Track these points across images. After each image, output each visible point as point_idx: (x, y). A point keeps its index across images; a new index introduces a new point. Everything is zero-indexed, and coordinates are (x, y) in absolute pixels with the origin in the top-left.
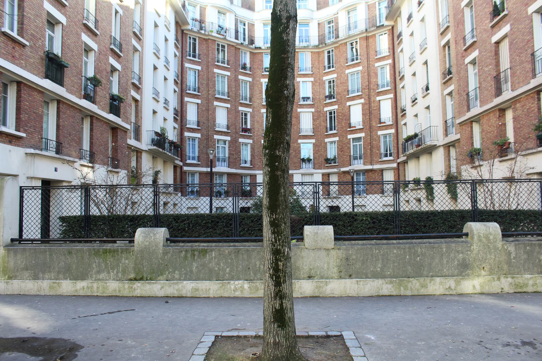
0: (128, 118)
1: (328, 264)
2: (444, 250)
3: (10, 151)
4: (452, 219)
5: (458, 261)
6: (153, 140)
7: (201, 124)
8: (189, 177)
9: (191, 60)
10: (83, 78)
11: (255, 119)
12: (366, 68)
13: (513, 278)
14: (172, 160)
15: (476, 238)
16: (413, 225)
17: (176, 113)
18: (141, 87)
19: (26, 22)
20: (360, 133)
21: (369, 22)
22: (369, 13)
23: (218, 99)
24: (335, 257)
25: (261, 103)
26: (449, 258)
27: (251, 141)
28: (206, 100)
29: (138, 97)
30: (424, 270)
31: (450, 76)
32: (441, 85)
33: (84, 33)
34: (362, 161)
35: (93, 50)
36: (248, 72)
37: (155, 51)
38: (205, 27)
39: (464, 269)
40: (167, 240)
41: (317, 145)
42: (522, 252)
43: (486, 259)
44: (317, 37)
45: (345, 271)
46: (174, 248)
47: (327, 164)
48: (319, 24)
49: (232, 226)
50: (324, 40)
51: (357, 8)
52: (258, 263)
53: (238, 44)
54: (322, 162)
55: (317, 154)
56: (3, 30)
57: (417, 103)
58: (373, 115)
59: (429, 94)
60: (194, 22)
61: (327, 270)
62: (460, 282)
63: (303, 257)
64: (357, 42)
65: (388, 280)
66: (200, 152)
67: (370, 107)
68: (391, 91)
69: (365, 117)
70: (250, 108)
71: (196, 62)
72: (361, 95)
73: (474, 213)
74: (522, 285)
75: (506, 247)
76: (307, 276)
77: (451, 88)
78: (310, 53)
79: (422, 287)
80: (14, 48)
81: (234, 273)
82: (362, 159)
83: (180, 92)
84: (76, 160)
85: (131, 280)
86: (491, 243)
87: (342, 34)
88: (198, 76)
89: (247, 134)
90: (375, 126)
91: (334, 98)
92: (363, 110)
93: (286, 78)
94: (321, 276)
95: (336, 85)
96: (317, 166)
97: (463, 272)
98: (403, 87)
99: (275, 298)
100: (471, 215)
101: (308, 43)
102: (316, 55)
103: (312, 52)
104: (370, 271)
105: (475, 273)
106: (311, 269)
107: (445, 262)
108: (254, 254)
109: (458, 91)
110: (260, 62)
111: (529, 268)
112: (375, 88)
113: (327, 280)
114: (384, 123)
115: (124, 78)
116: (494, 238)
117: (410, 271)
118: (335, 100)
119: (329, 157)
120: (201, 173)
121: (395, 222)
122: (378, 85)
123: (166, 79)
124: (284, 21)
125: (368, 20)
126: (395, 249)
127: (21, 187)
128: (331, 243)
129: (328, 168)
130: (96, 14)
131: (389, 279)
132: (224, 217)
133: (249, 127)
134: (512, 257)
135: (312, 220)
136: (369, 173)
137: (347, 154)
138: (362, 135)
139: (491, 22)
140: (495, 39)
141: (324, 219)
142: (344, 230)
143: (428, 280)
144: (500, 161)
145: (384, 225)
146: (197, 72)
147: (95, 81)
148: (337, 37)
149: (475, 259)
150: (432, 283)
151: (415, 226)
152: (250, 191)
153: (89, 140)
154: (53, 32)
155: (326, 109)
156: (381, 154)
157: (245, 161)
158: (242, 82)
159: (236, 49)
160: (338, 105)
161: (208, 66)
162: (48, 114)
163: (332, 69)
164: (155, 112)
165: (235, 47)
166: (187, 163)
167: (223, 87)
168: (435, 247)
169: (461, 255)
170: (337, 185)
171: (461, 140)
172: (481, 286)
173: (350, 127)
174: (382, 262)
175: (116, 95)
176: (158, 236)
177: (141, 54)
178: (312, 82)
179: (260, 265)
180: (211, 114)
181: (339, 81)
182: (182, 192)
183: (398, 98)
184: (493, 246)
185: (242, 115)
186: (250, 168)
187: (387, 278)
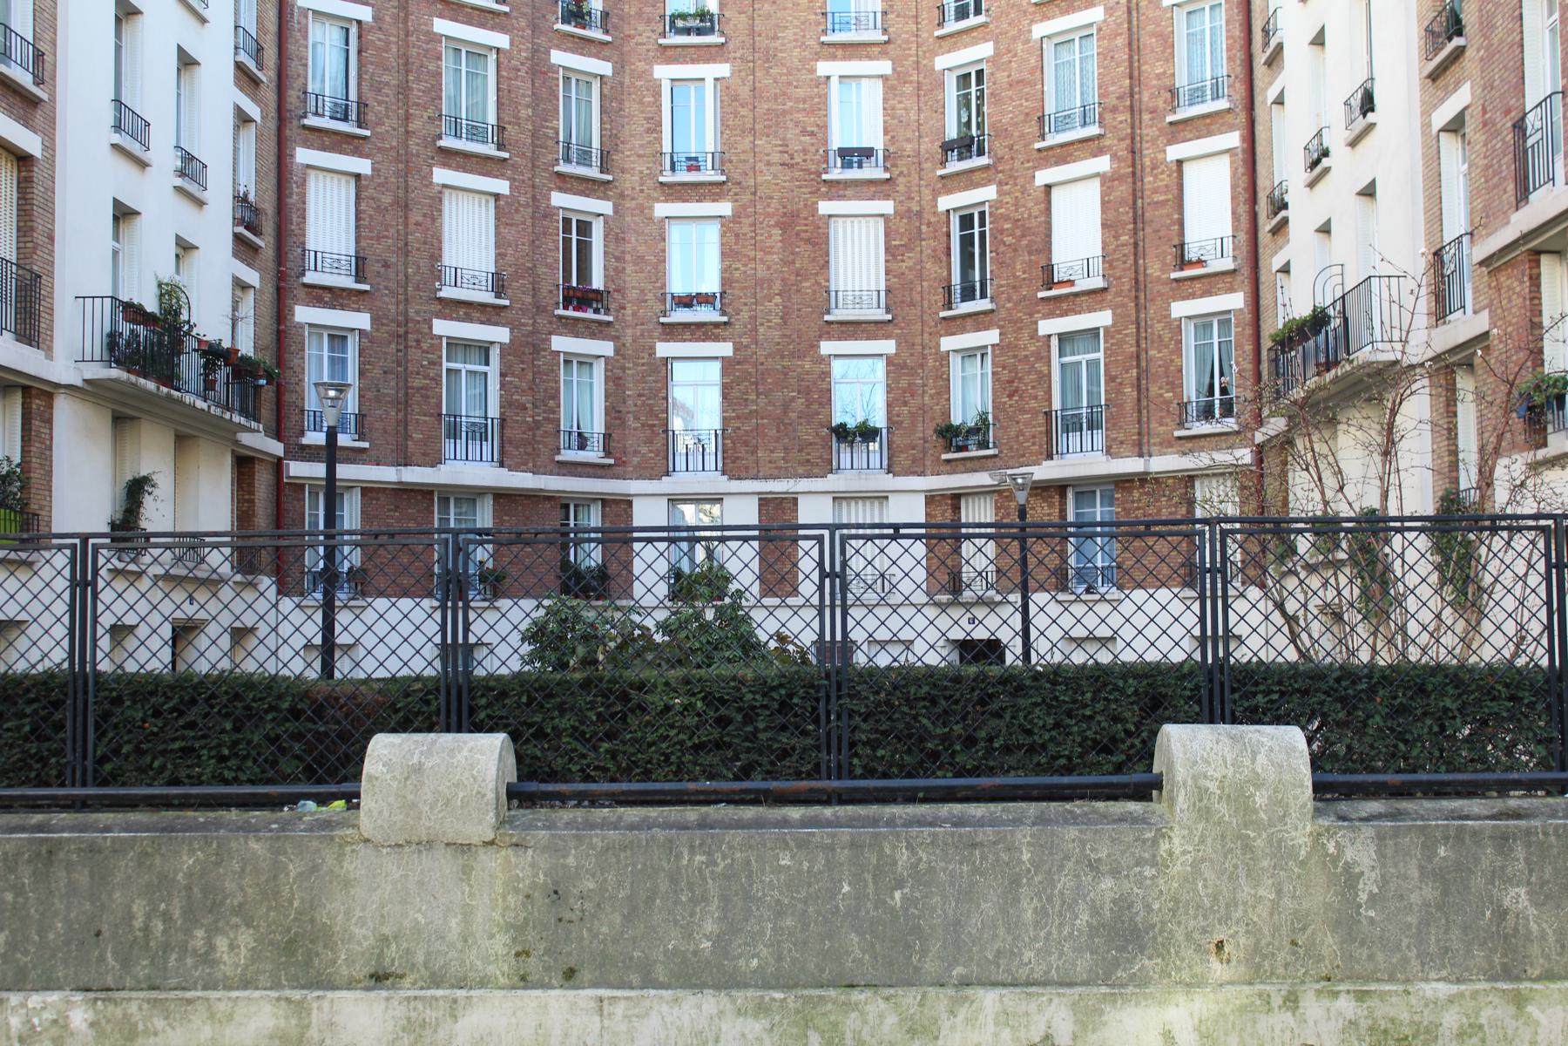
1: (467, 914)
2: (1026, 856)
4: (1099, 706)
5: (1095, 910)
6: (112, 340)
7: (373, 267)
11: (628, 247)
12: (1121, 12)
13: (1361, 996)
14: (227, 434)
15: (1182, 801)
16: (910, 736)
17: (247, 215)
18: (44, 96)
23: (451, 158)
24: (499, 882)
25: (652, 176)
26: (1050, 899)
27: (606, 348)
28: (397, 160)
29: (30, 142)
30: (924, 952)
31: (1457, 41)
32: (1423, 89)
34: (1099, 436)
36: (596, 34)
39: (1121, 949)
41: (904, 366)
42: (1414, 872)
43: (1233, 903)
45: (547, 952)
47: (948, 449)
49: (61, 735)
52: (139, 908)
54: (925, 441)
55: (905, 404)
57: (1327, 170)
58: (1148, 230)
59: (1371, 126)
61: (459, 945)
62: (1102, 1013)
63: (347, 884)
66: (369, 395)
68: (1229, 118)
69: (1117, 237)
70: (606, 198)
72: (1099, 137)
73: (1211, 681)
74: (1407, 1031)
75: (1331, 849)
76: (367, 970)
77: (1461, 98)
79: (912, 1032)
81: (26, 953)
82: (1099, 427)
83: (272, 125)
86: (1259, 826)
88: (360, 52)
89: (590, 315)
90: (1158, 279)
91: (981, 153)
92: (1105, 205)
94: (433, 974)
96: (903, 460)
97: (1116, 964)
98: (1279, 101)
100: (1197, 688)
104: (666, 952)
105: (1179, 969)
106: (384, 940)
107: (1029, 915)
108: (125, 865)
109: (1484, 112)
111: (1447, 950)
113: (461, 993)
114: (1200, 263)
116: (1275, 802)
117: (858, 953)
118: (984, 160)
119: (956, 420)
121: (823, 718)
122: (1173, 92)
123: (186, 62)
126: (786, 846)
128: (482, 826)
129: (952, 467)
131: (750, 993)
132: (28, 690)
133: (597, 282)
134: (1363, 897)
135: (433, 708)
136: (1130, 490)
137: (1033, 404)
141: (489, 705)
142: (584, 756)
143: (939, 999)
145: (769, 735)
146: (354, 30)
149: (1176, 901)
150: (961, 1017)
151: (921, 739)
152: (602, 574)
155: (945, 202)
156: (1183, 406)
157: (580, 434)
158: (567, 79)
160: (1000, 184)
163: (973, 21)
164: (123, 214)
166: (304, 447)
167: (478, 106)
168: (982, 844)
169: (1107, 883)
170: (989, 537)
172: (1202, 1036)
173: (1050, 283)
174: (724, 910)
178: (884, 78)
179: (148, 917)
180: (418, 224)
181: (1002, 76)
183: (1259, 149)
184: (1270, 842)
185: (567, 229)
186: (603, 466)
187: (746, 986)
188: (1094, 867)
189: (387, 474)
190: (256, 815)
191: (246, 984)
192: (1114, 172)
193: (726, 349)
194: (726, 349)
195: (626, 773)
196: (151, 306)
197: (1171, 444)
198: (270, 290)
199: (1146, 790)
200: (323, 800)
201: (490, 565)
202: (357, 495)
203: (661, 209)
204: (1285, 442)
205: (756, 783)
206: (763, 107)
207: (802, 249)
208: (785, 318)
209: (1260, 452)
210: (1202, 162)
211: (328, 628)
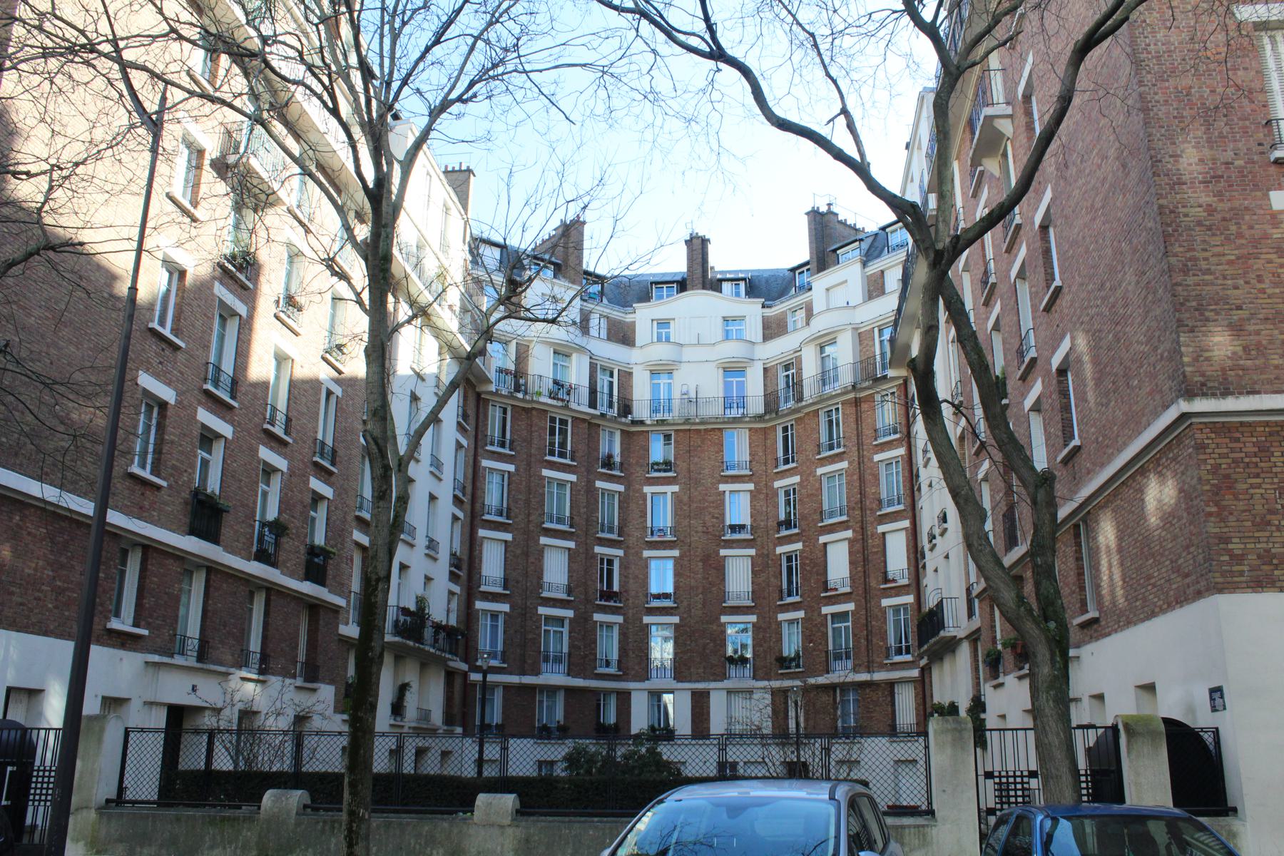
0: (343, 584)
1: (502, 846)
3: (121, 659)
9: (493, 452)
11: (631, 571)
12: (856, 464)
17: (456, 562)
19: (166, 449)
20: (845, 603)
21: (862, 369)
22: (861, 351)
27: (620, 619)
34: (850, 664)
41: (760, 628)
47: (781, 668)
48: (765, 370)
52: (412, 842)
53: (593, 416)
55: (761, 646)
56: (151, 325)
60: (502, 376)
64: (837, 409)
67: (864, 548)
68: (905, 514)
70: (620, 548)
71: (505, 455)
72: (847, 521)
78: (747, 431)
80: (143, 494)
83: (468, 519)
84: (232, 670)
87: (809, 392)
89: (612, 604)
92: (850, 553)
95: (800, 500)
96: (760, 673)
102: (761, 437)
103: (750, 429)
110: (642, 452)
112: (874, 506)
115: (338, 512)
118: (796, 531)
119: (785, 654)
122: (880, 501)
123: (432, 498)
127: (126, 728)
129: (783, 676)
130: (288, 407)
138: (850, 607)
146: (506, 476)
147: (278, 528)
148: (801, 399)
153: (261, 630)
154: (210, 453)
155: (779, 550)
156: (888, 649)
158: (603, 494)
159: (590, 427)
161: (529, 464)
162: (190, 591)
165: (590, 423)
176: (291, 800)
182: (464, 726)
185: (602, 563)
189: (514, 679)
190: (445, 816)
193: (676, 620)
194: (676, 620)
195: (551, 807)
196: (413, 608)
197: (883, 667)
198: (465, 594)
201: (562, 723)
202: (501, 689)
203: (646, 553)
208: (704, 605)
210: (894, 534)
211: (481, 752)
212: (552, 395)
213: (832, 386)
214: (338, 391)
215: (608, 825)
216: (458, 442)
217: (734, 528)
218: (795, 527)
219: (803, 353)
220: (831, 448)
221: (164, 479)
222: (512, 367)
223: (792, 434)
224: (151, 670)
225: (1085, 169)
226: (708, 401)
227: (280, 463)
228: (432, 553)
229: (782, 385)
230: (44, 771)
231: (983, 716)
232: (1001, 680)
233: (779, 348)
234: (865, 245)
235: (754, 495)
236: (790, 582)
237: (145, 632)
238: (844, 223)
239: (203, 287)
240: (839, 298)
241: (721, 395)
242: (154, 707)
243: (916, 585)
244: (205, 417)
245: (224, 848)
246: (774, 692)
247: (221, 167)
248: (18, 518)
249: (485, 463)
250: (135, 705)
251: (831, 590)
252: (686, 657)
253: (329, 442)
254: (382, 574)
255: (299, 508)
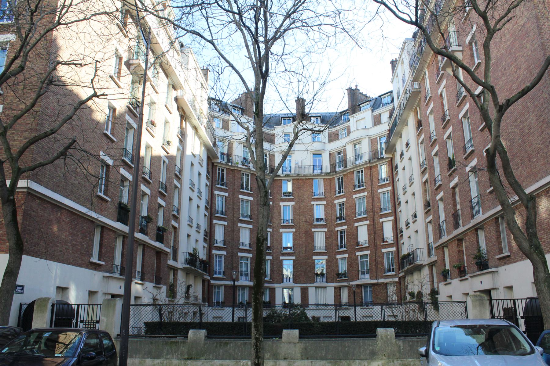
5: (370, 351)
6: (186, 260)
8: (215, 289)
9: (219, 188)
10: (140, 217)
12: (370, 193)
13: (401, 361)
14: (202, 275)
29: (176, 225)
31: (429, 208)
33: (142, 183)
34: (368, 276)
35: (147, 194)
37: (190, 186)
38: (232, 160)
40: (206, 337)
41: (329, 261)
42: (407, 345)
43: (385, 350)
44: (329, 166)
46: (210, 341)
47: (338, 278)
48: (330, 154)
50: (335, 168)
51: (362, 142)
57: (409, 227)
59: (416, 220)
60: (223, 156)
65: (328, 361)
67: (374, 228)
69: (371, 236)
71: (224, 189)
77: (430, 218)
83: (210, 216)
85: (185, 359)
87: (350, 164)
91: (344, 219)
92: (368, 230)
93: (262, 265)
96: (329, 280)
99: (256, 359)
101: (320, 171)
102: (328, 182)
103: (324, 179)
106: (285, 354)
110: (279, 188)
112: (378, 211)
114: (387, 242)
118: (344, 221)
119: (340, 272)
120: (226, 286)
122: (381, 209)
123: (198, 207)
124: (262, 241)
125: (371, 153)
128: (297, 340)
129: (339, 281)
130: (150, 167)
138: (368, 252)
139: (448, 172)
140: (452, 185)
143: (352, 361)
144: (461, 281)
146: (224, 198)
147: (148, 219)
148: (346, 167)
155: (337, 229)
156: (385, 270)
160: (348, 226)
161: (234, 193)
163: (342, 194)
164: (189, 236)
169: (371, 347)
171: (438, 261)
175: (161, 227)
176: (201, 334)
177: (180, 190)
181: (347, 205)
182: (208, 302)
183: (397, 220)
188: (369, 345)
191: (269, 359)
192: (370, 224)
194: (294, 258)
198: (208, 247)
199: (375, 336)
200: (276, 338)
203: (281, 230)
204: (404, 277)
205: (328, 336)
206: (301, 210)
207: (309, 238)
209: (400, 278)
210: (387, 222)
212: (243, 164)
213: (360, 161)
214: (167, 161)
215: (340, 341)
216: (206, 183)
217: (318, 220)
218: (344, 219)
219: (347, 147)
220: (359, 187)
221: (109, 197)
222: (226, 152)
223: (342, 181)
224: (105, 279)
225: (506, 73)
226: (306, 167)
227: (148, 191)
228: (198, 230)
229: (337, 161)
230: (88, 322)
231: (437, 296)
232: (449, 281)
233: (336, 145)
234: (372, 103)
235: (326, 206)
236: (341, 243)
237: (103, 263)
238: (361, 94)
239: (122, 115)
240: (361, 125)
241: (312, 164)
242: (107, 295)
243: (397, 243)
244: (123, 171)
245: (173, 355)
246: (335, 288)
247: (128, 65)
248: (59, 214)
249: (216, 192)
250: (100, 294)
251: (360, 245)
252: (298, 273)
253: (164, 183)
254: (265, 237)
255: (154, 211)
